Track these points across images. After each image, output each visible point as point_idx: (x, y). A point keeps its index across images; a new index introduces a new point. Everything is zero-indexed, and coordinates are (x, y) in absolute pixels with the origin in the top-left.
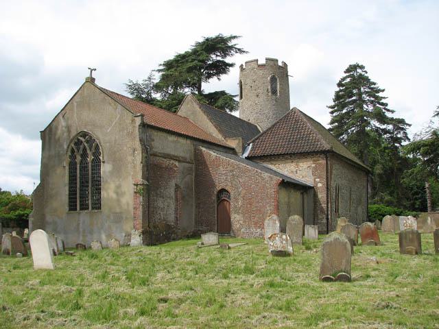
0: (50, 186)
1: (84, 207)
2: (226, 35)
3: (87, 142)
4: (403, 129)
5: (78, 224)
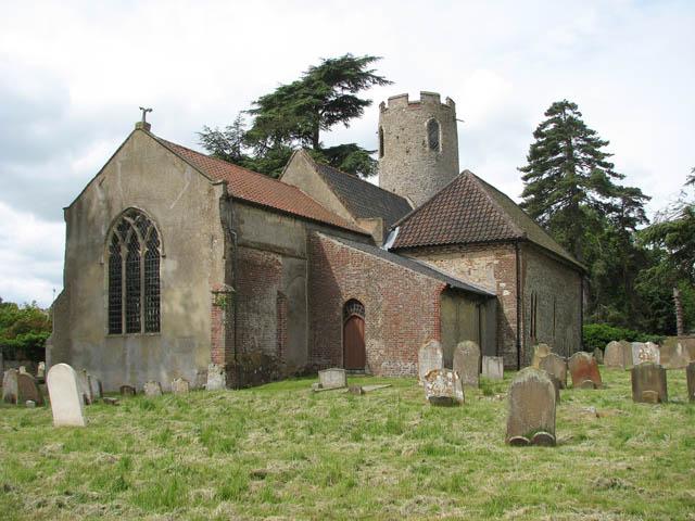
0: (79, 294)
1: (133, 328)
2: (358, 55)
3: (138, 225)
4: (637, 204)
5: (124, 355)
